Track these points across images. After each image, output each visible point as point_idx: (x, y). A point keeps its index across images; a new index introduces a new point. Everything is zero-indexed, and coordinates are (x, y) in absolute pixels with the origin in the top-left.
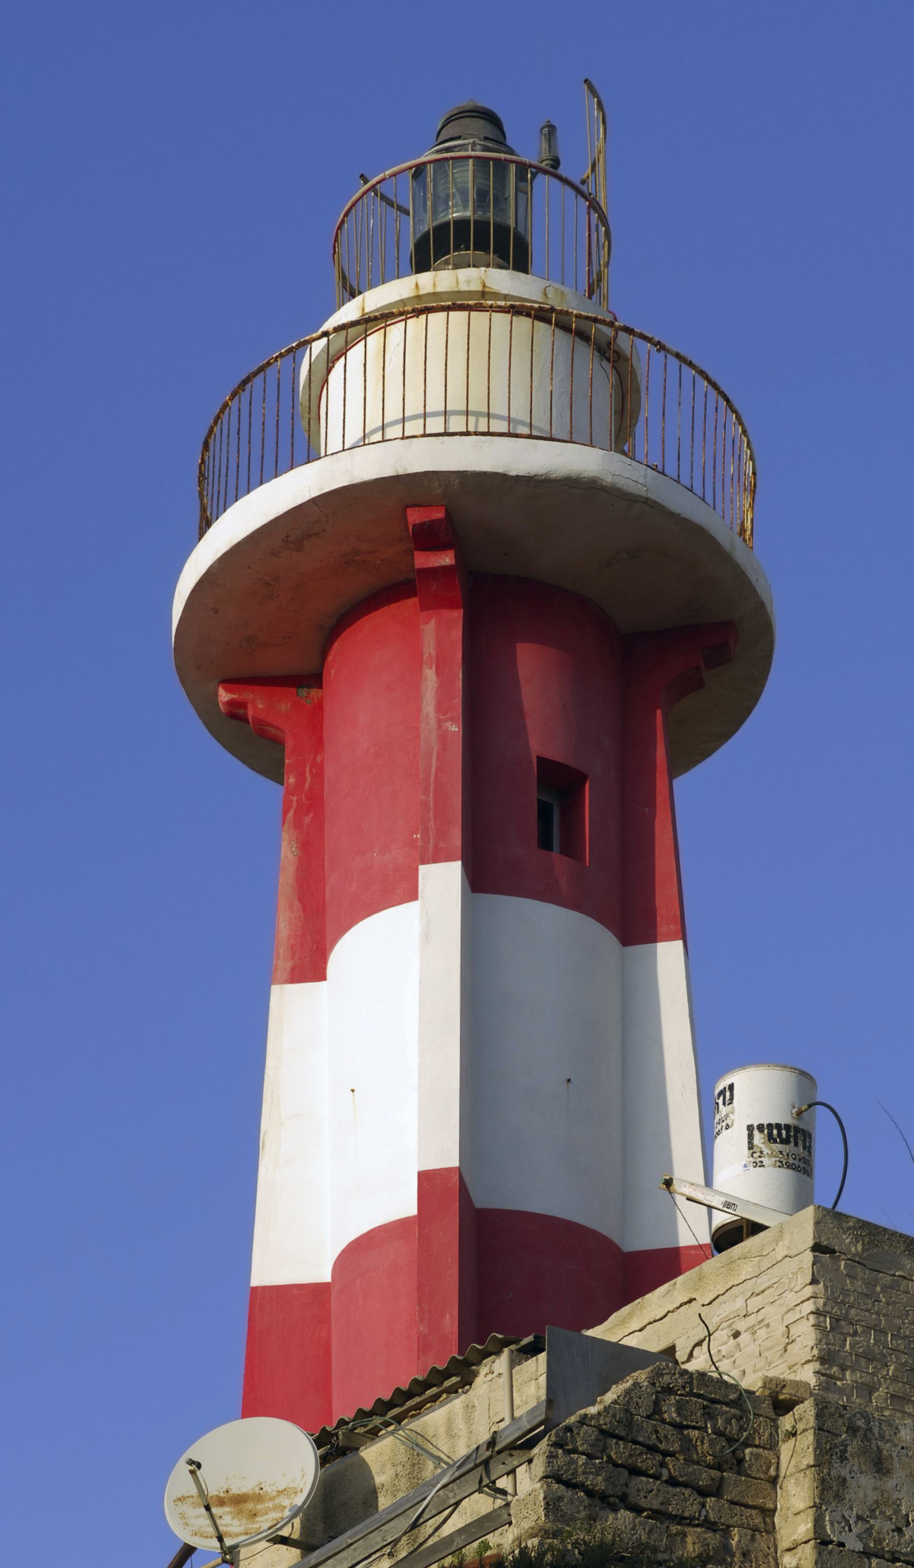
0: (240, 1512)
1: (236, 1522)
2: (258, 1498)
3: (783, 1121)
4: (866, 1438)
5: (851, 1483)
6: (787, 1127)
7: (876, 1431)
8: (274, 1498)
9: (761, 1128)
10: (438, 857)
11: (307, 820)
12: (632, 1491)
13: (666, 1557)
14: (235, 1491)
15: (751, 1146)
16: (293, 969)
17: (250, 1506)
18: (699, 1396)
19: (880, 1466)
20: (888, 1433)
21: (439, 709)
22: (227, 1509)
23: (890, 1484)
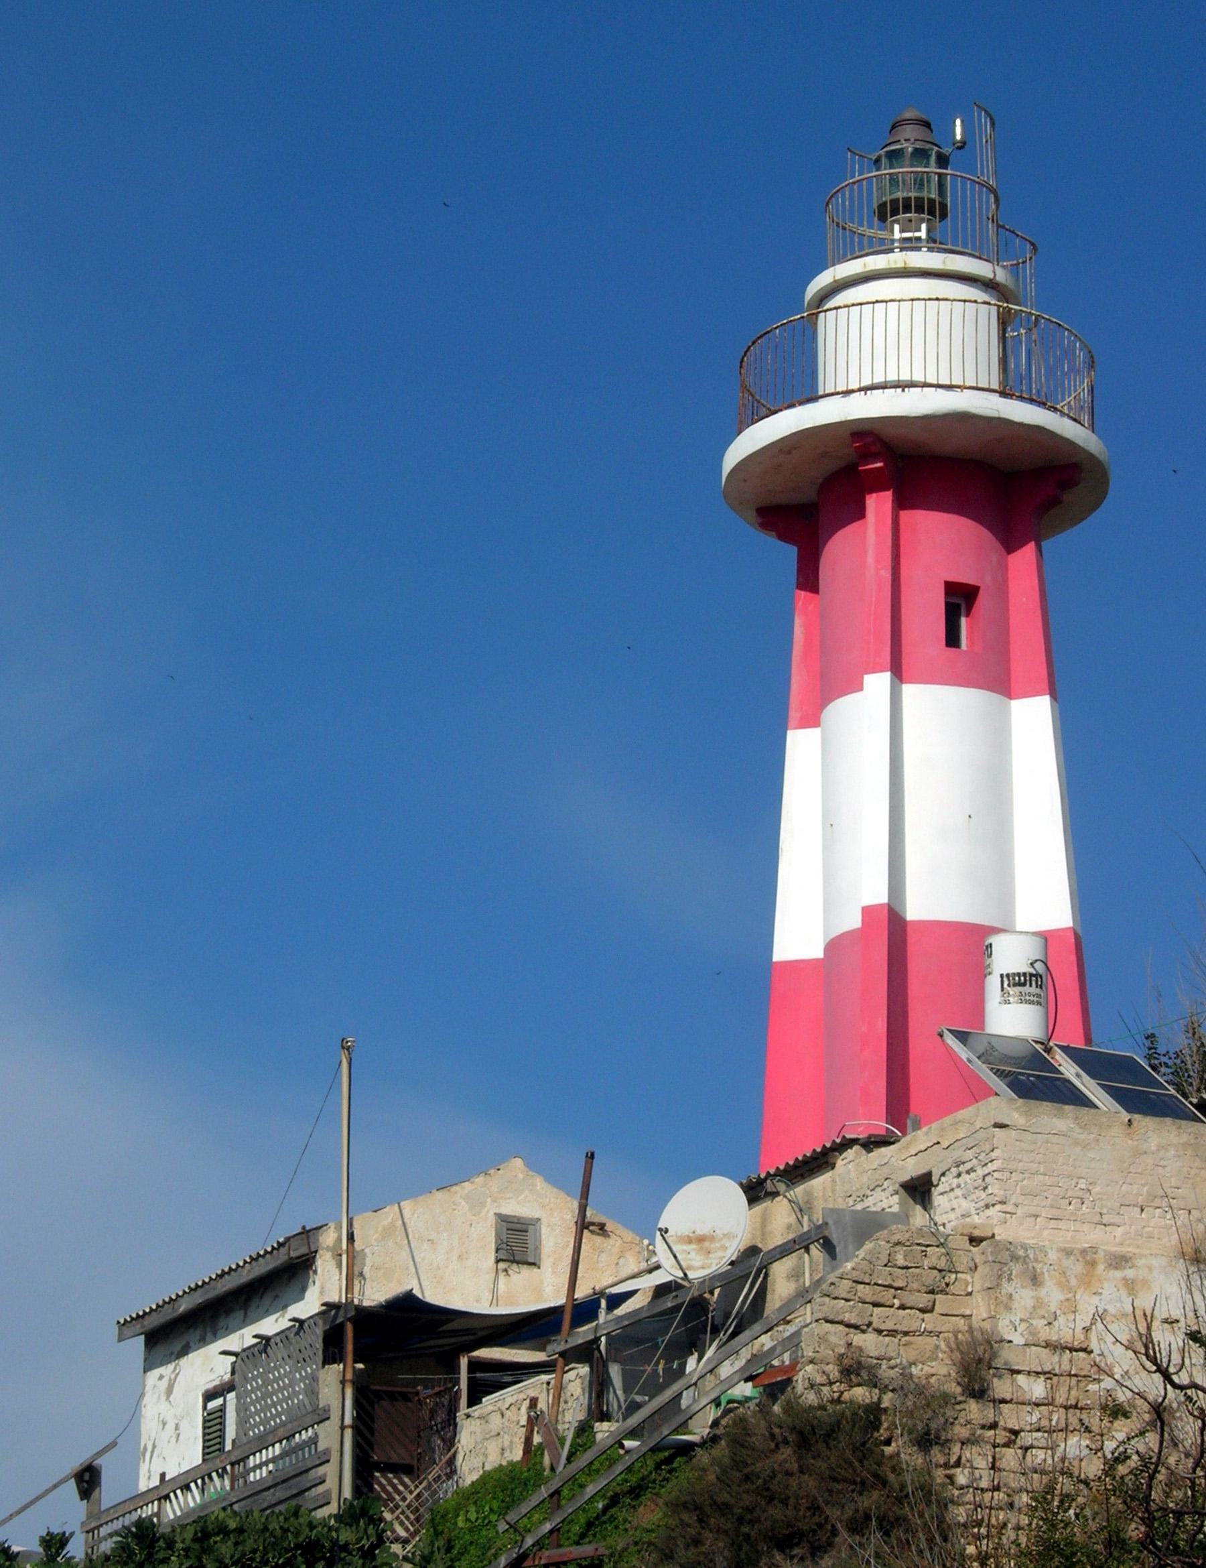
0: (701, 1249)
1: (698, 1258)
2: (712, 1238)
3: (1021, 970)
4: (1025, 1262)
5: (1016, 1296)
6: (1024, 974)
7: (1031, 1256)
8: (720, 1240)
9: (1008, 975)
10: (875, 670)
11: (811, 607)
12: (875, 1320)
13: (898, 1361)
14: (699, 1232)
15: (1003, 989)
16: (802, 718)
17: (707, 1244)
18: (918, 1244)
19: (1035, 1280)
20: (1040, 1256)
21: (877, 561)
22: (693, 1246)
23: (1043, 1292)
